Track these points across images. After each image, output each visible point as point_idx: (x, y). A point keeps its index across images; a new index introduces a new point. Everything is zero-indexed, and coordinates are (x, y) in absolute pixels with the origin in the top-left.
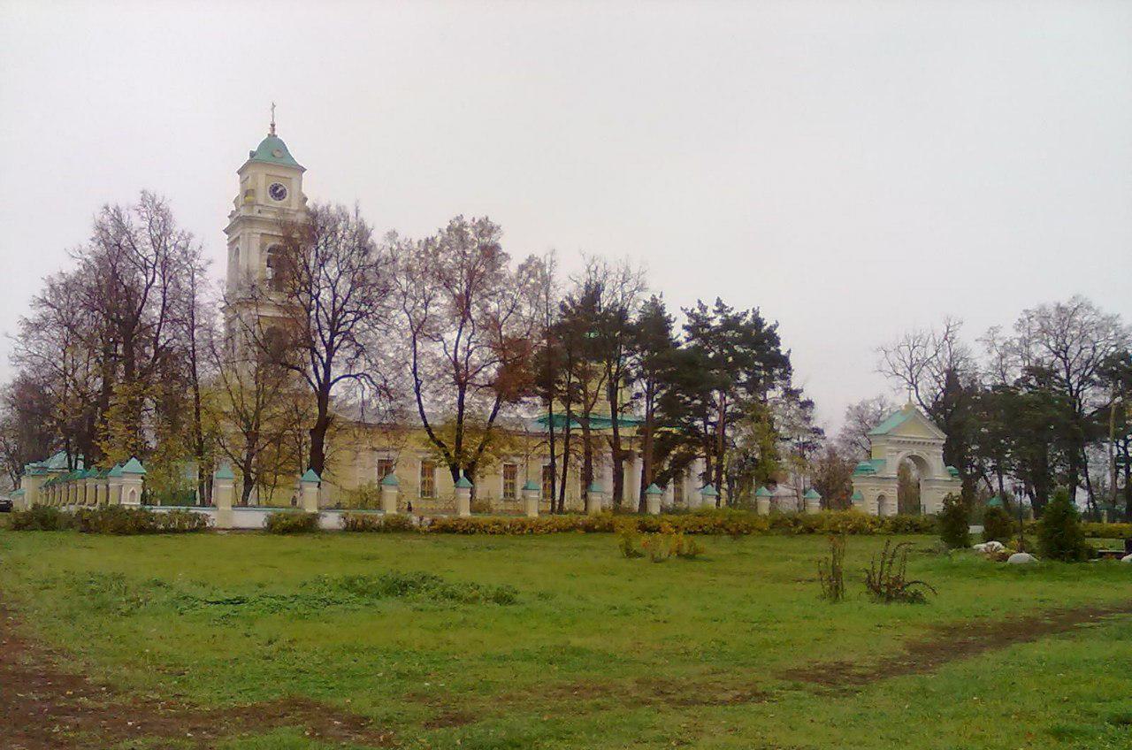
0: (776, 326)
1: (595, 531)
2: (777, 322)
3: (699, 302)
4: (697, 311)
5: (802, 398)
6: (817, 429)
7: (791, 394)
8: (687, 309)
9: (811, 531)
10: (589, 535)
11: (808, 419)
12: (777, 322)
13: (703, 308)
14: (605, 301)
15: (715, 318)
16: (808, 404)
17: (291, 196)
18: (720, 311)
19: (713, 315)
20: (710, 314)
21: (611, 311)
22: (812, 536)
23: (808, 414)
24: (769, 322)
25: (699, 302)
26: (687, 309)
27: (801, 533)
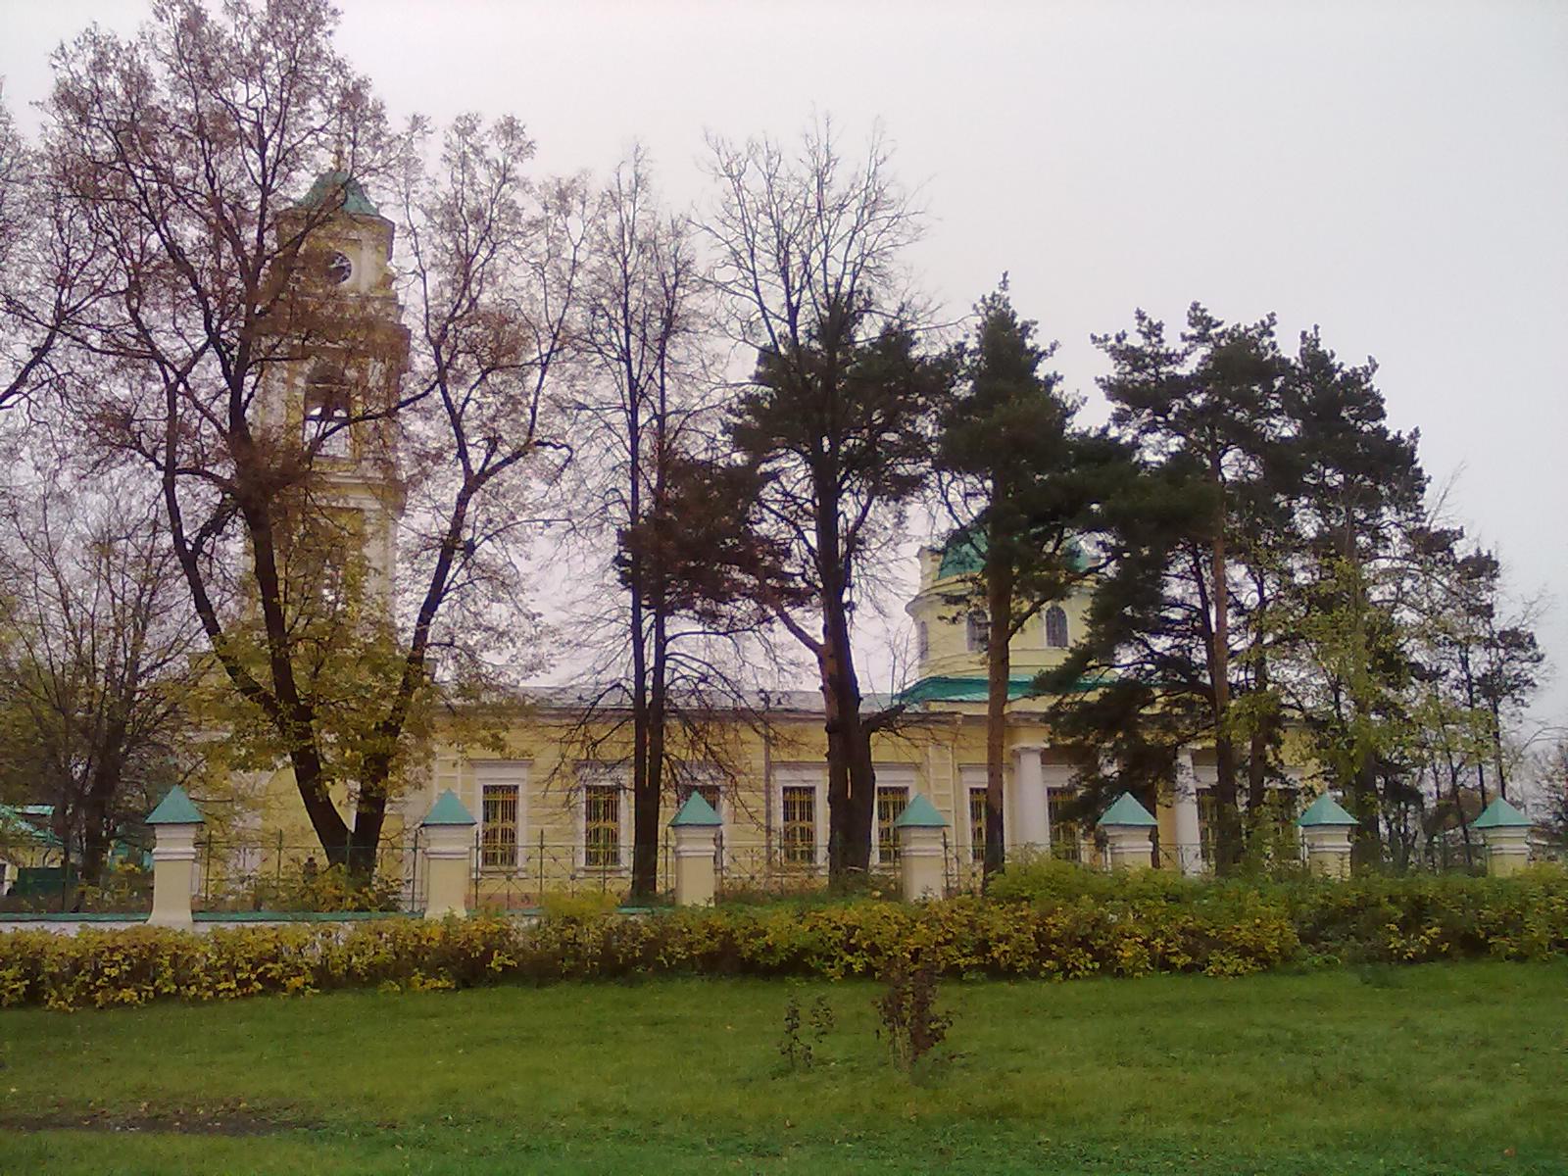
0: (1368, 372)
1: (495, 980)
2: (1370, 359)
3: (1141, 317)
4: (1136, 341)
5: (1462, 550)
6: (1514, 632)
7: (1432, 545)
8: (1106, 338)
9: (1472, 946)
10: (475, 997)
11: (1488, 612)
12: (1370, 359)
13: (1154, 331)
14: (1056, 390)
15: (1186, 353)
16: (1483, 567)
17: (359, 275)
18: (1202, 338)
19: (1180, 347)
20: (1173, 343)
21: (845, 353)
22: (1481, 969)
23: (1487, 597)
24: (1347, 358)
25: (1141, 317)
26: (1106, 338)
27: (1432, 955)
